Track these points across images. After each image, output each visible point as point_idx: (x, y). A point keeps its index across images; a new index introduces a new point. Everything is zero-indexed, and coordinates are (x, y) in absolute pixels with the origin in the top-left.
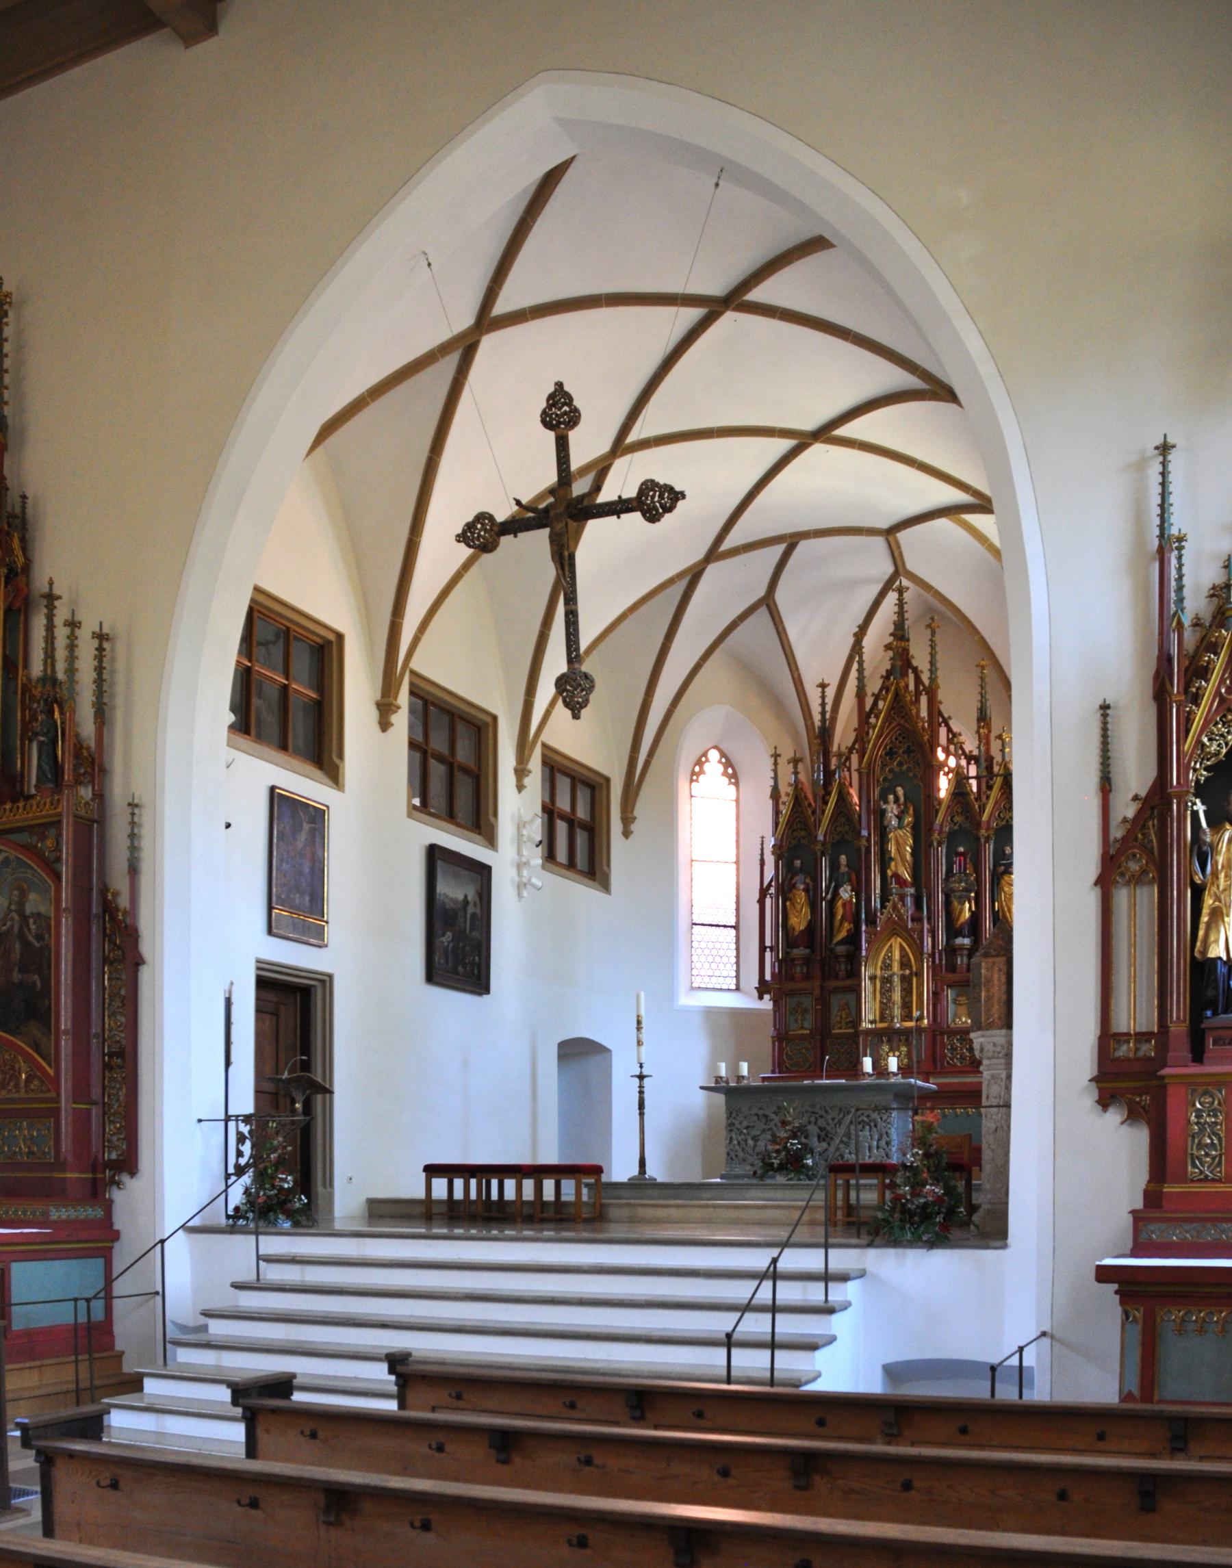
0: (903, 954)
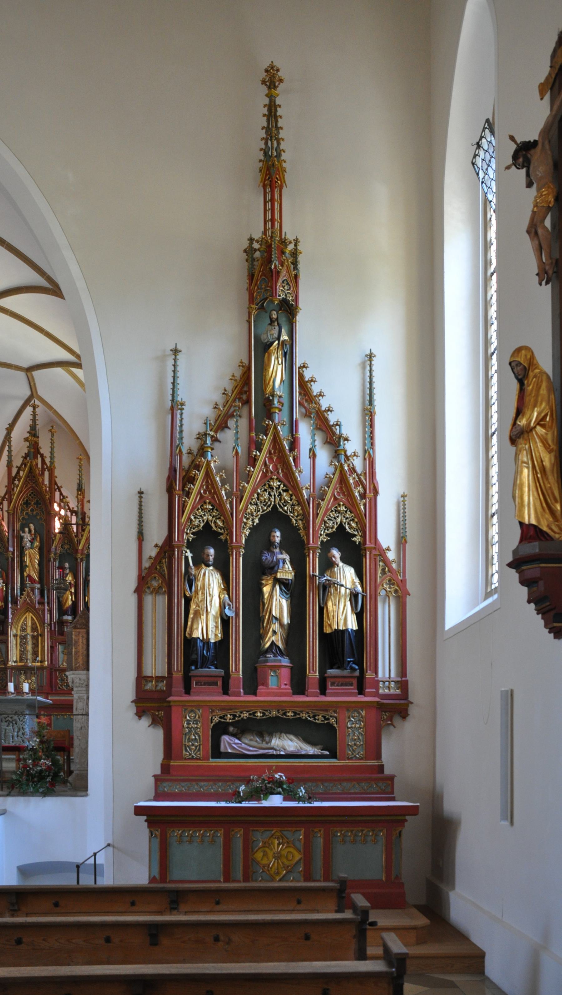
0: (33, 623)
